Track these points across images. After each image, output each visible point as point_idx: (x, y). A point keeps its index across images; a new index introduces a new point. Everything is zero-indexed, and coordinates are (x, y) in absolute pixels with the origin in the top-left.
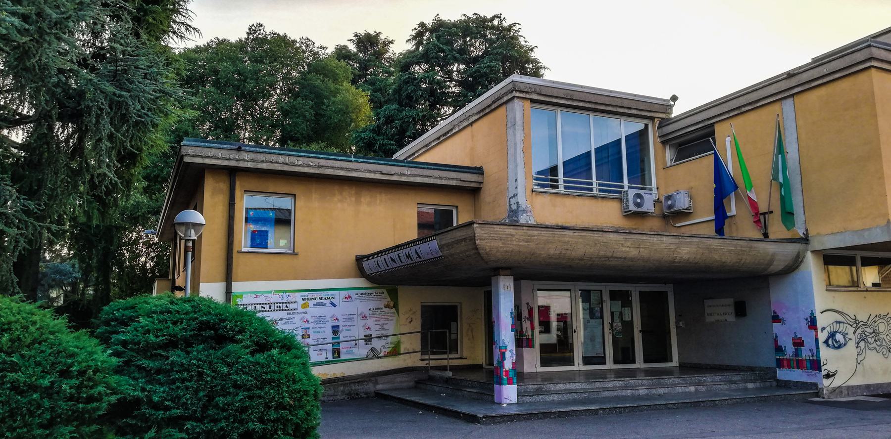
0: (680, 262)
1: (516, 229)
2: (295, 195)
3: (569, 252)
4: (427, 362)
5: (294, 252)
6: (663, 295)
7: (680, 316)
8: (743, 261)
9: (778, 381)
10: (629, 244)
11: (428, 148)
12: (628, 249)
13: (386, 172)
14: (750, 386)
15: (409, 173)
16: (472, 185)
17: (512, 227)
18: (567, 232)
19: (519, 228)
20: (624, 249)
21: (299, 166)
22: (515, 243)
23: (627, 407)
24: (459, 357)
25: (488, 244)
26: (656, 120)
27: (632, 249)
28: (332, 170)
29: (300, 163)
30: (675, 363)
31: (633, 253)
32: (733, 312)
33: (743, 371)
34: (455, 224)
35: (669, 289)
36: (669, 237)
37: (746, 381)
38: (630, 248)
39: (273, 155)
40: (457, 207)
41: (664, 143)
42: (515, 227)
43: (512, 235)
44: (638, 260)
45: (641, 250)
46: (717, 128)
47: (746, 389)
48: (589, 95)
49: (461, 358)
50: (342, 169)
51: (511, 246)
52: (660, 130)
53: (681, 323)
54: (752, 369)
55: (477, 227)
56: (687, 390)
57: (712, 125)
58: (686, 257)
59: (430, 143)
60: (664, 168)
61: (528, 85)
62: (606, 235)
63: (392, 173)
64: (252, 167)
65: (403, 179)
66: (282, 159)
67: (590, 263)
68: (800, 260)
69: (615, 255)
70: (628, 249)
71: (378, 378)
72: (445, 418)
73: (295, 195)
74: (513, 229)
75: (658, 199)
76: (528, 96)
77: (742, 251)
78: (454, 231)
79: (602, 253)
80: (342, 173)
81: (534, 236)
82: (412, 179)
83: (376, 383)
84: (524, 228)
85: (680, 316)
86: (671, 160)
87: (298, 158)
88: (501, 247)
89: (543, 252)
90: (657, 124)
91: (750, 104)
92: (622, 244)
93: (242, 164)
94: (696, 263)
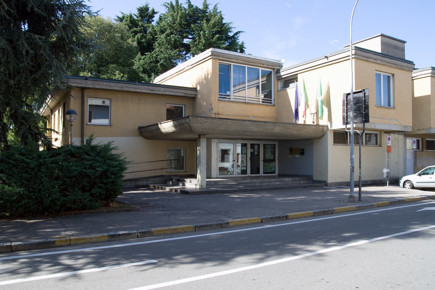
0: (275, 133)
1: (207, 119)
2: (111, 99)
3: (229, 129)
4: (170, 173)
5: (111, 125)
6: (274, 145)
7: (280, 155)
8: (301, 133)
9: (313, 180)
10: (254, 126)
11: (172, 76)
12: (253, 128)
13: (152, 90)
14: (302, 182)
15: (163, 90)
16: (192, 96)
17: (205, 118)
18: (228, 121)
19: (209, 119)
20: (252, 128)
21: (113, 87)
22: (207, 125)
23: (249, 189)
24: (184, 171)
25: (195, 125)
26: (275, 69)
27: (255, 128)
28: (128, 89)
29: (114, 85)
30: (277, 173)
31: (256, 129)
32: (426, 148)
33: (300, 177)
34: (184, 116)
35: (276, 143)
36: (271, 123)
37: (300, 180)
38: (254, 127)
39: (102, 82)
40: (185, 105)
41: (278, 80)
42: (207, 119)
43: (206, 122)
44: (258, 132)
45: (259, 128)
46: (299, 76)
47: (300, 183)
48: (245, 58)
49: (185, 172)
50: (132, 88)
51: (205, 126)
52: (277, 74)
53: (280, 157)
54: (304, 176)
55: (191, 118)
56: (276, 184)
57: (297, 74)
58: (278, 131)
59: (173, 74)
60: (277, 91)
61: (217, 53)
62: (245, 122)
63: (155, 90)
64: (92, 87)
65: (160, 93)
66: (105, 84)
67: (238, 133)
68: (324, 133)
69: (248, 130)
70: (253, 128)
71: (148, 179)
72: (236, 258)
73: (111, 99)
74: (206, 119)
75: (274, 105)
76: (218, 58)
77: (301, 129)
78: (181, 119)
79: (243, 129)
80: (132, 90)
81: (215, 122)
82: (164, 93)
83: (148, 181)
84: (211, 119)
85: (280, 155)
86: (281, 88)
87: (113, 83)
88: (201, 127)
89: (218, 129)
90: (275, 72)
91: (312, 67)
92: (251, 126)
93: (87, 86)
94: (282, 134)
